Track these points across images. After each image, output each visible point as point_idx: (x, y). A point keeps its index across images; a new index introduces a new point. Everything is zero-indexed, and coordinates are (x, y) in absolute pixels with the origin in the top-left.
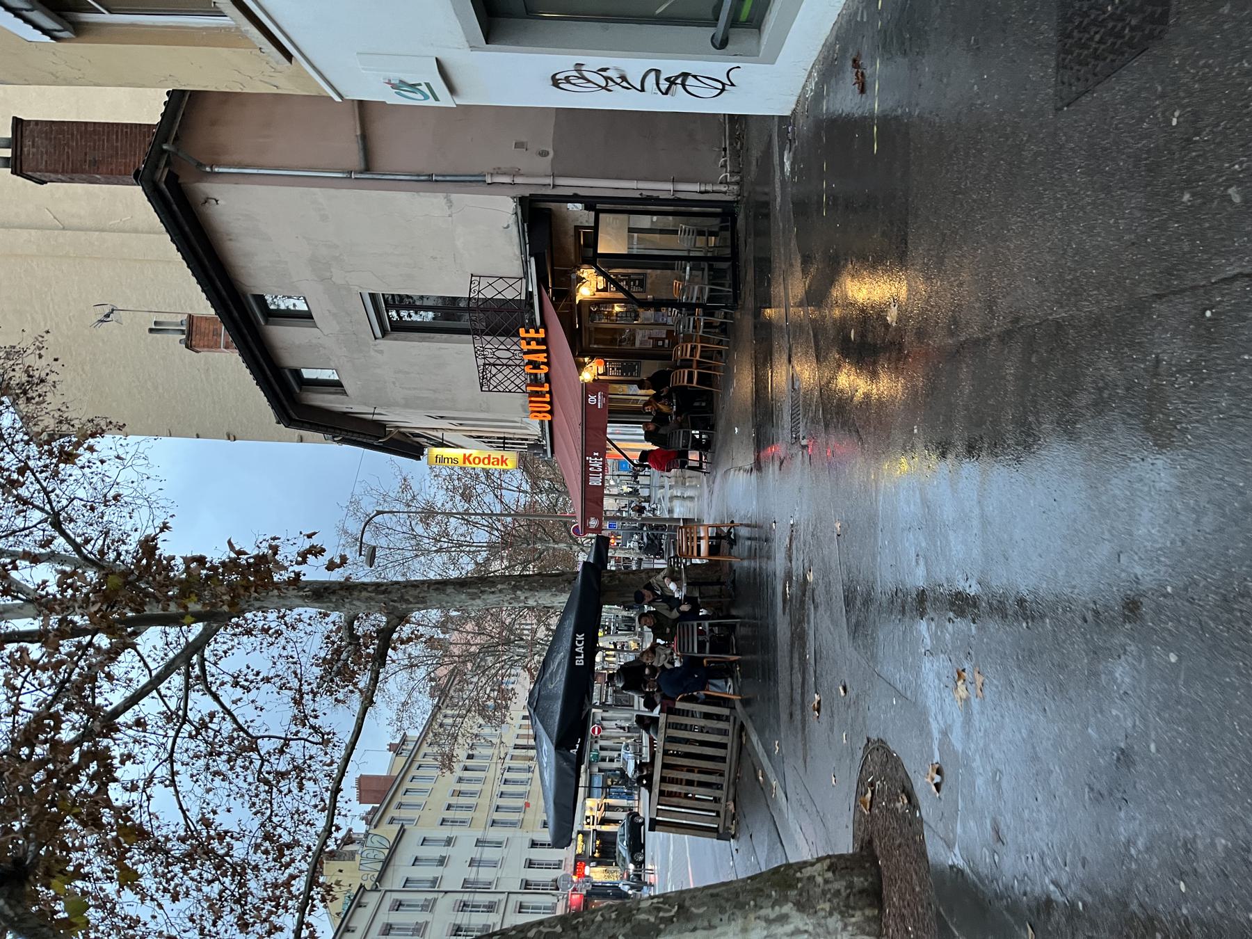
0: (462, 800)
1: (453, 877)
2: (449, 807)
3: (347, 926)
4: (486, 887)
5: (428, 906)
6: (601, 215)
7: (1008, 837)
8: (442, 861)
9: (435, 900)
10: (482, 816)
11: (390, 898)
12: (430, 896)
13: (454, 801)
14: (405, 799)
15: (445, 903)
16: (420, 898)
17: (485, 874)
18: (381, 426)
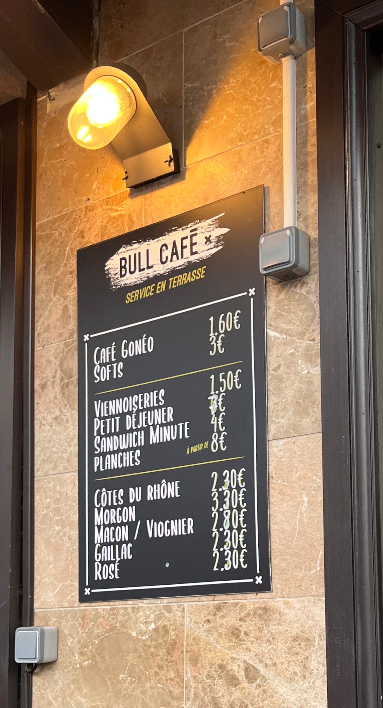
6: (217, 396)
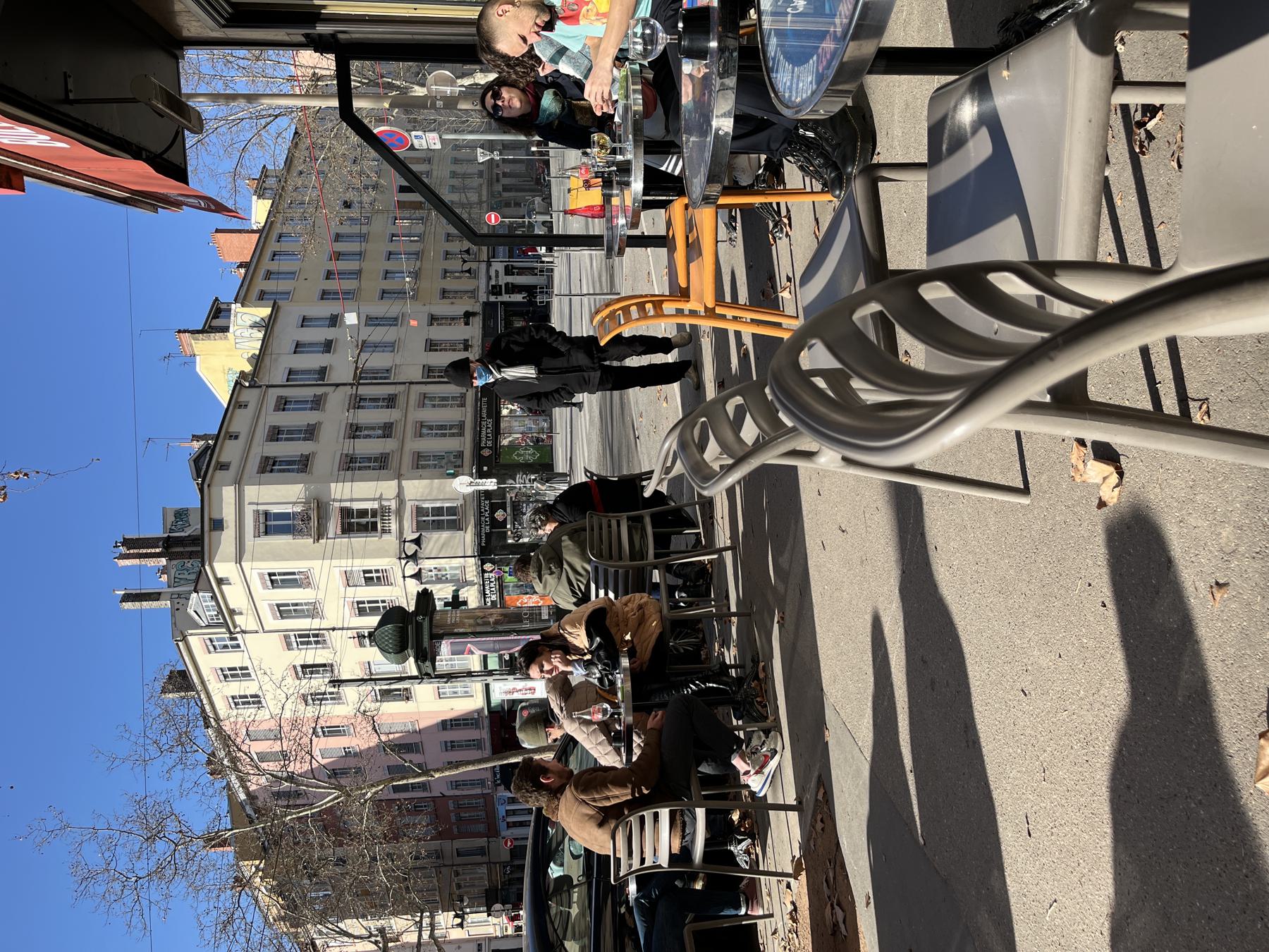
0: (342, 265)
1: (342, 366)
2: (329, 275)
3: (237, 402)
4: (380, 377)
5: (317, 403)
7: (1112, 160)
8: (328, 346)
9: (326, 395)
10: (373, 284)
11: (273, 394)
12: (319, 391)
13: (332, 266)
14: (274, 266)
15: (337, 400)
16: (308, 393)
17: (377, 361)
18: (100, 130)
